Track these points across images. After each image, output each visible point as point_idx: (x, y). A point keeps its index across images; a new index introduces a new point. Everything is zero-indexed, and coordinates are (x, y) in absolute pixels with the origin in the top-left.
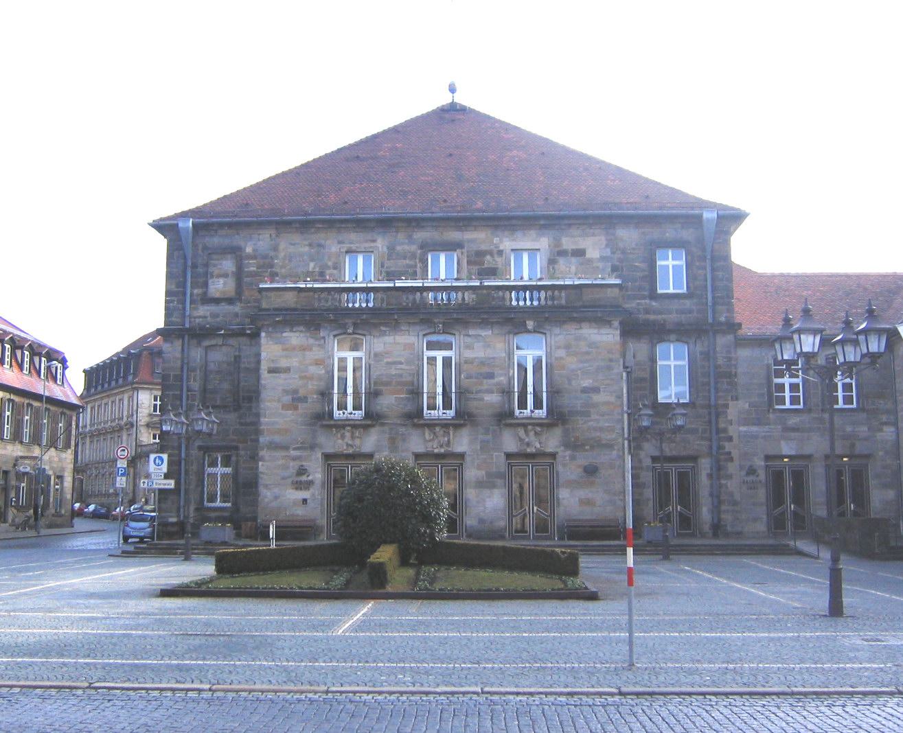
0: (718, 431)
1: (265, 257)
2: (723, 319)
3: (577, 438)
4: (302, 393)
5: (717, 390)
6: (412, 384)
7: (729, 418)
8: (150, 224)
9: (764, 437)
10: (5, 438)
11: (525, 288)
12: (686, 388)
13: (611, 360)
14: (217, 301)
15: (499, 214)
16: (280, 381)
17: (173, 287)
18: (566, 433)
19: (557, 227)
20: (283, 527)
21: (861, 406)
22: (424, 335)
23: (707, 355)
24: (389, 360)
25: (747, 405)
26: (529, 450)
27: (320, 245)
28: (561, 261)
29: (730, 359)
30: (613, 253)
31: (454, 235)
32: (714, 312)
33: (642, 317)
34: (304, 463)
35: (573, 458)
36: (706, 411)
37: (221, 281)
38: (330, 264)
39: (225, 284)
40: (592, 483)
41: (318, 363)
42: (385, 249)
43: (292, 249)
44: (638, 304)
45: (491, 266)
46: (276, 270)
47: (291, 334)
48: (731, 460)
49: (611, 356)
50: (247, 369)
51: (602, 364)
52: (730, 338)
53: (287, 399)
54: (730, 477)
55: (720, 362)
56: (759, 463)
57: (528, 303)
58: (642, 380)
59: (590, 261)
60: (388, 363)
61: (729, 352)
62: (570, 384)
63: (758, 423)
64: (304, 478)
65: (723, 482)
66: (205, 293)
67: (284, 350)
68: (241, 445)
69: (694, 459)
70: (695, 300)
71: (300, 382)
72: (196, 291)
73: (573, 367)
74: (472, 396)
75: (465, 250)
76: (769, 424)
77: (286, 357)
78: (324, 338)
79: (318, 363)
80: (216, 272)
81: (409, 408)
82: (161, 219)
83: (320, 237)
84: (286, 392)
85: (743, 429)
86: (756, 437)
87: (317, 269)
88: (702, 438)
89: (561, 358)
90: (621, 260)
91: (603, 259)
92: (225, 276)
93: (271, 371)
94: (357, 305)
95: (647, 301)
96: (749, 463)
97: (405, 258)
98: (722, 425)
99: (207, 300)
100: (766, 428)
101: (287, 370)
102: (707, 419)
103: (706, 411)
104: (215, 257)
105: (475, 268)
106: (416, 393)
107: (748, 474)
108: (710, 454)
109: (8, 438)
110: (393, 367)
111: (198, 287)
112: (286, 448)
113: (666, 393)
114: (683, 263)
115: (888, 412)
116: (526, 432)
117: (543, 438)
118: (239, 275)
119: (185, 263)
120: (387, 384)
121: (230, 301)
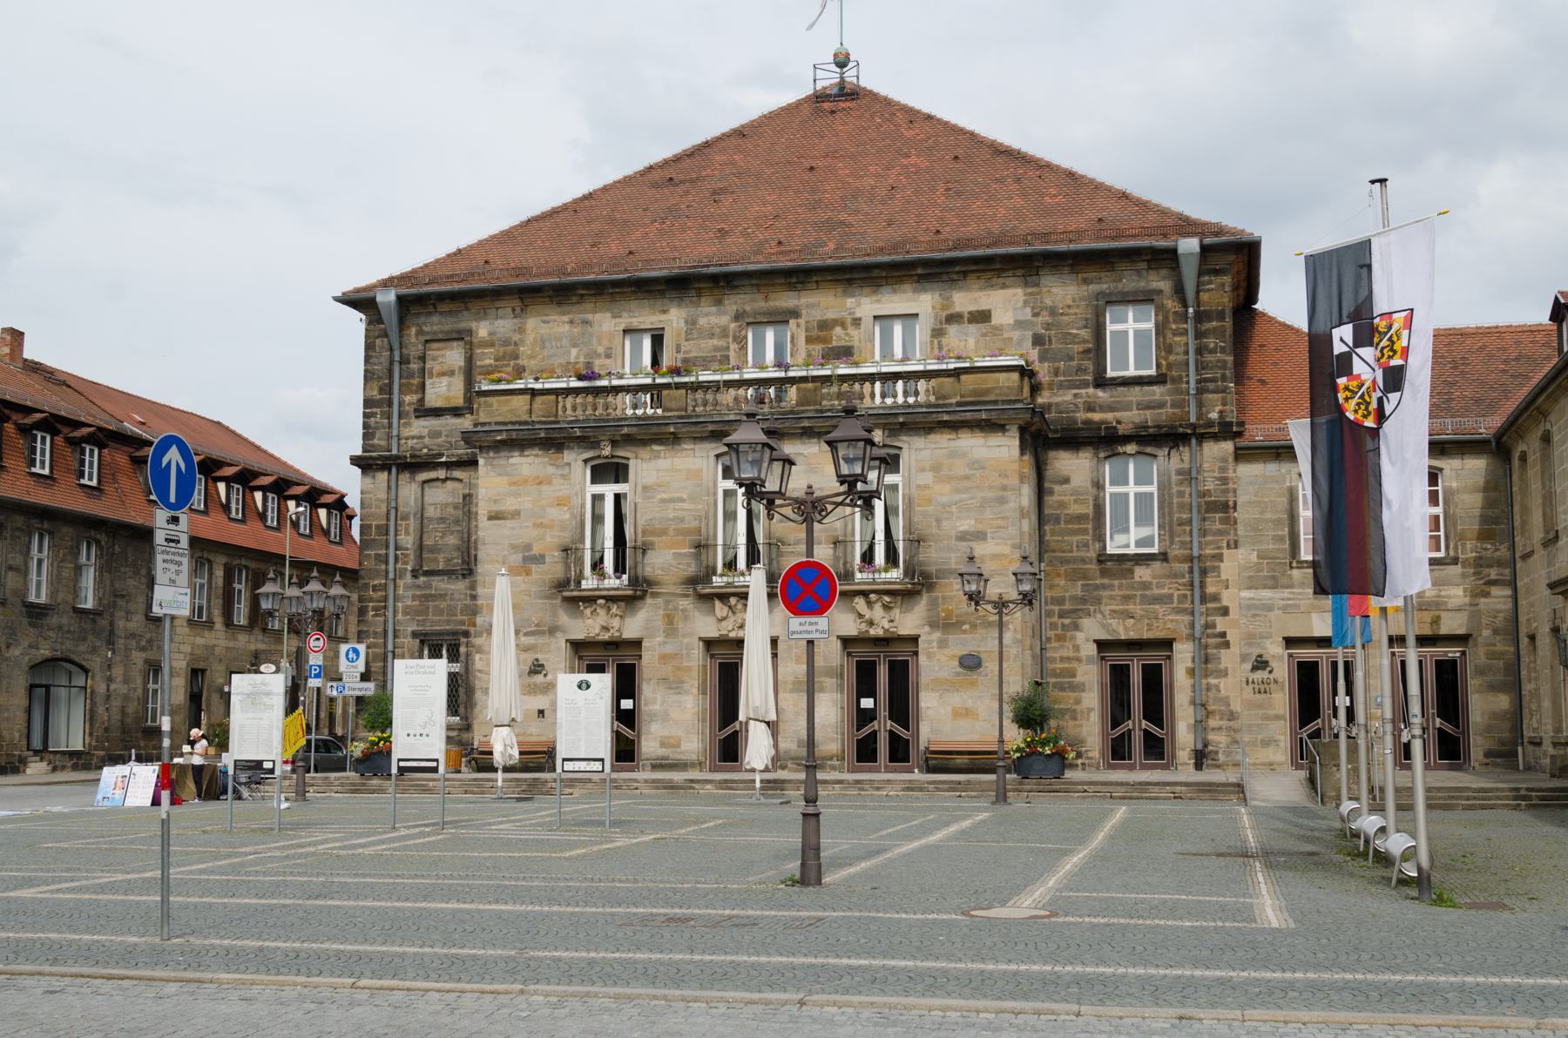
0: (1204, 599)
1: (506, 343)
2: (1214, 415)
3: (949, 613)
4: (536, 550)
5: (1203, 533)
6: (699, 531)
7: (1223, 577)
8: (337, 299)
9: (1285, 609)
11: (896, 376)
12: (1154, 531)
13: (1004, 488)
14: (437, 412)
16: (505, 529)
17: (375, 392)
18: (933, 604)
19: (945, 277)
20: (1439, 789)
21: (1452, 553)
22: (718, 456)
23: (1188, 476)
24: (665, 496)
25: (1254, 557)
26: (872, 632)
27: (585, 322)
28: (953, 330)
29: (1224, 481)
30: (1035, 315)
31: (785, 300)
32: (1200, 405)
33: (1081, 416)
34: (539, 656)
35: (943, 644)
36: (1186, 566)
37: (445, 380)
38: (601, 350)
39: (449, 385)
40: (973, 684)
41: (560, 502)
42: (682, 324)
44: (1075, 395)
45: (843, 343)
47: (523, 460)
48: (1227, 645)
49: (1005, 482)
51: (990, 494)
52: (1228, 446)
53: (516, 558)
54: (1224, 673)
55: (1210, 486)
56: (1274, 649)
57: (878, 400)
58: (1080, 518)
59: (998, 329)
60: (663, 501)
61: (1223, 469)
62: (939, 527)
63: (1274, 583)
64: (539, 678)
65: (1213, 681)
66: (422, 400)
69: (1167, 644)
70: (1169, 386)
71: (535, 533)
72: (408, 399)
73: (944, 500)
74: (790, 549)
75: (802, 321)
76: (1291, 586)
77: (516, 495)
78: (569, 464)
79: (560, 502)
80: (437, 368)
81: (692, 570)
82: (358, 291)
84: (514, 547)
85: (1245, 594)
86: (1270, 608)
87: (582, 359)
88: (1178, 611)
89: (927, 487)
90: (1048, 326)
91: (1019, 324)
93: (495, 517)
94: (900, 400)
95: (1091, 390)
96: (1255, 651)
97: (712, 336)
98: (1210, 589)
99: (424, 412)
100: (1286, 593)
101: (516, 514)
102: (1186, 580)
103: (1186, 566)
104: (435, 345)
105: (818, 349)
106: (702, 546)
107: (1254, 669)
108: (1192, 637)
110: (671, 506)
111: (411, 392)
113: (1120, 539)
114: (1150, 325)
115: (1499, 563)
116: (870, 604)
117: (896, 613)
118: (469, 373)
119: (392, 356)
120: (663, 533)
121: (456, 412)
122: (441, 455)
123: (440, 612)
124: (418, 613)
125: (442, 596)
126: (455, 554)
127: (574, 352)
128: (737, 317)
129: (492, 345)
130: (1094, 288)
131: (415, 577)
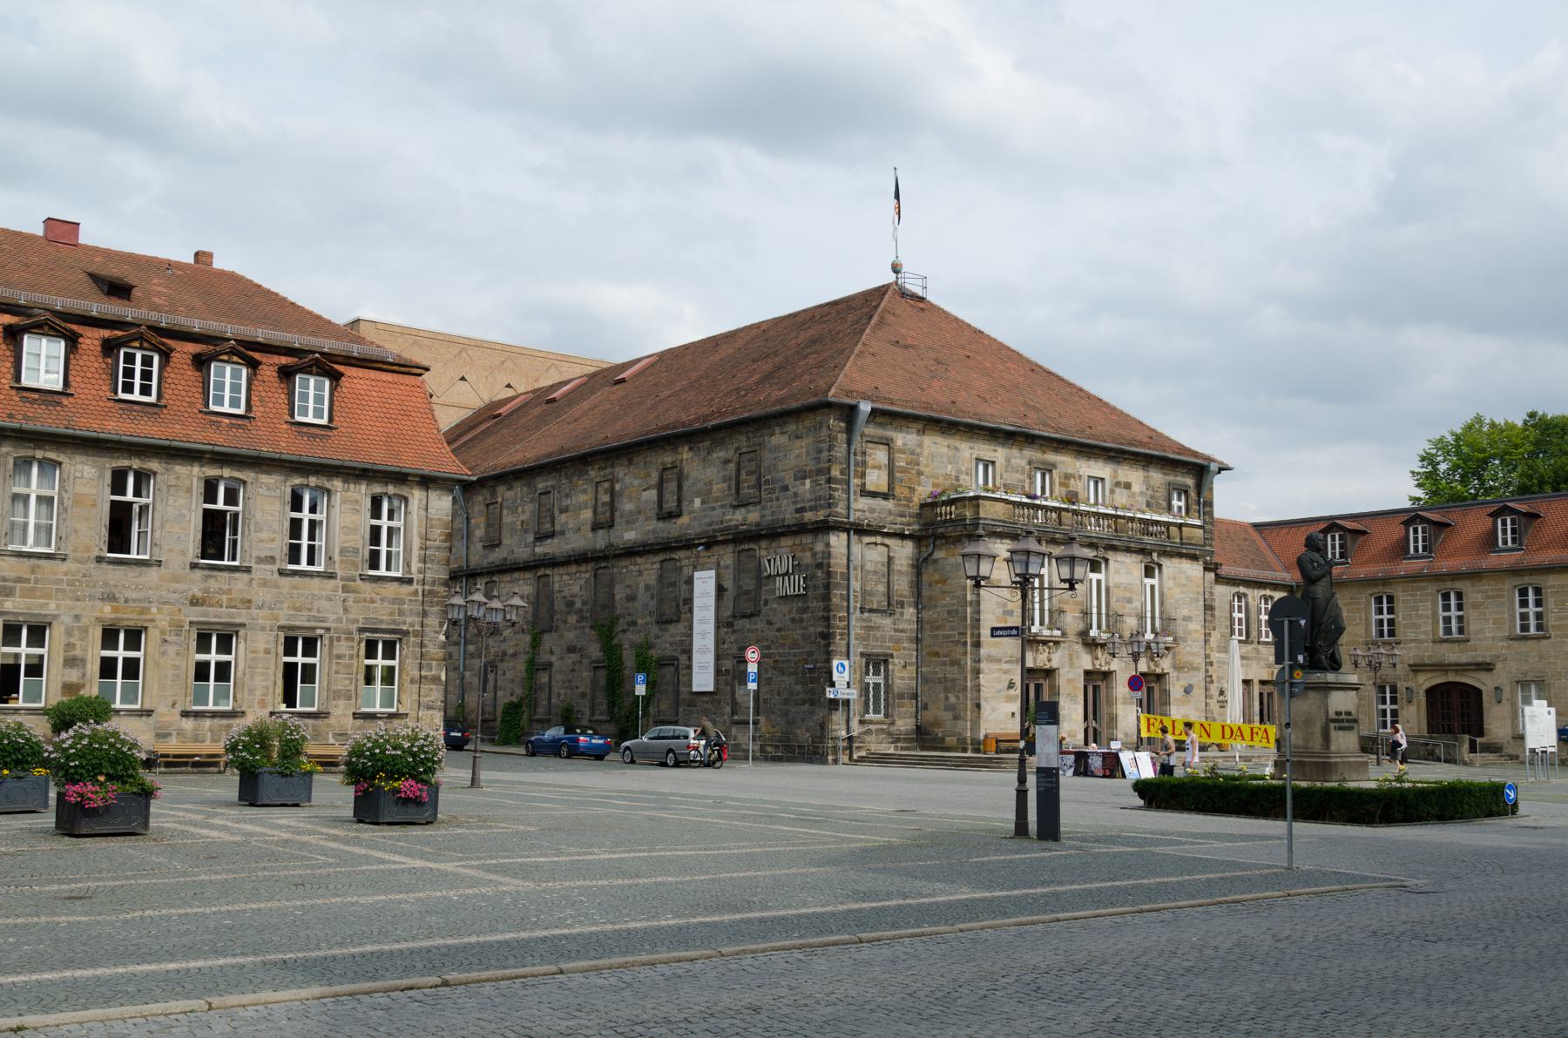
14: (874, 495)
28: (1118, 490)
37: (876, 472)
66: (864, 485)
91: (1142, 493)
92: (879, 468)
99: (865, 493)
112: (999, 661)
121: (885, 496)
124: (864, 639)
125: (877, 628)
128: (1030, 463)
130: (1171, 478)
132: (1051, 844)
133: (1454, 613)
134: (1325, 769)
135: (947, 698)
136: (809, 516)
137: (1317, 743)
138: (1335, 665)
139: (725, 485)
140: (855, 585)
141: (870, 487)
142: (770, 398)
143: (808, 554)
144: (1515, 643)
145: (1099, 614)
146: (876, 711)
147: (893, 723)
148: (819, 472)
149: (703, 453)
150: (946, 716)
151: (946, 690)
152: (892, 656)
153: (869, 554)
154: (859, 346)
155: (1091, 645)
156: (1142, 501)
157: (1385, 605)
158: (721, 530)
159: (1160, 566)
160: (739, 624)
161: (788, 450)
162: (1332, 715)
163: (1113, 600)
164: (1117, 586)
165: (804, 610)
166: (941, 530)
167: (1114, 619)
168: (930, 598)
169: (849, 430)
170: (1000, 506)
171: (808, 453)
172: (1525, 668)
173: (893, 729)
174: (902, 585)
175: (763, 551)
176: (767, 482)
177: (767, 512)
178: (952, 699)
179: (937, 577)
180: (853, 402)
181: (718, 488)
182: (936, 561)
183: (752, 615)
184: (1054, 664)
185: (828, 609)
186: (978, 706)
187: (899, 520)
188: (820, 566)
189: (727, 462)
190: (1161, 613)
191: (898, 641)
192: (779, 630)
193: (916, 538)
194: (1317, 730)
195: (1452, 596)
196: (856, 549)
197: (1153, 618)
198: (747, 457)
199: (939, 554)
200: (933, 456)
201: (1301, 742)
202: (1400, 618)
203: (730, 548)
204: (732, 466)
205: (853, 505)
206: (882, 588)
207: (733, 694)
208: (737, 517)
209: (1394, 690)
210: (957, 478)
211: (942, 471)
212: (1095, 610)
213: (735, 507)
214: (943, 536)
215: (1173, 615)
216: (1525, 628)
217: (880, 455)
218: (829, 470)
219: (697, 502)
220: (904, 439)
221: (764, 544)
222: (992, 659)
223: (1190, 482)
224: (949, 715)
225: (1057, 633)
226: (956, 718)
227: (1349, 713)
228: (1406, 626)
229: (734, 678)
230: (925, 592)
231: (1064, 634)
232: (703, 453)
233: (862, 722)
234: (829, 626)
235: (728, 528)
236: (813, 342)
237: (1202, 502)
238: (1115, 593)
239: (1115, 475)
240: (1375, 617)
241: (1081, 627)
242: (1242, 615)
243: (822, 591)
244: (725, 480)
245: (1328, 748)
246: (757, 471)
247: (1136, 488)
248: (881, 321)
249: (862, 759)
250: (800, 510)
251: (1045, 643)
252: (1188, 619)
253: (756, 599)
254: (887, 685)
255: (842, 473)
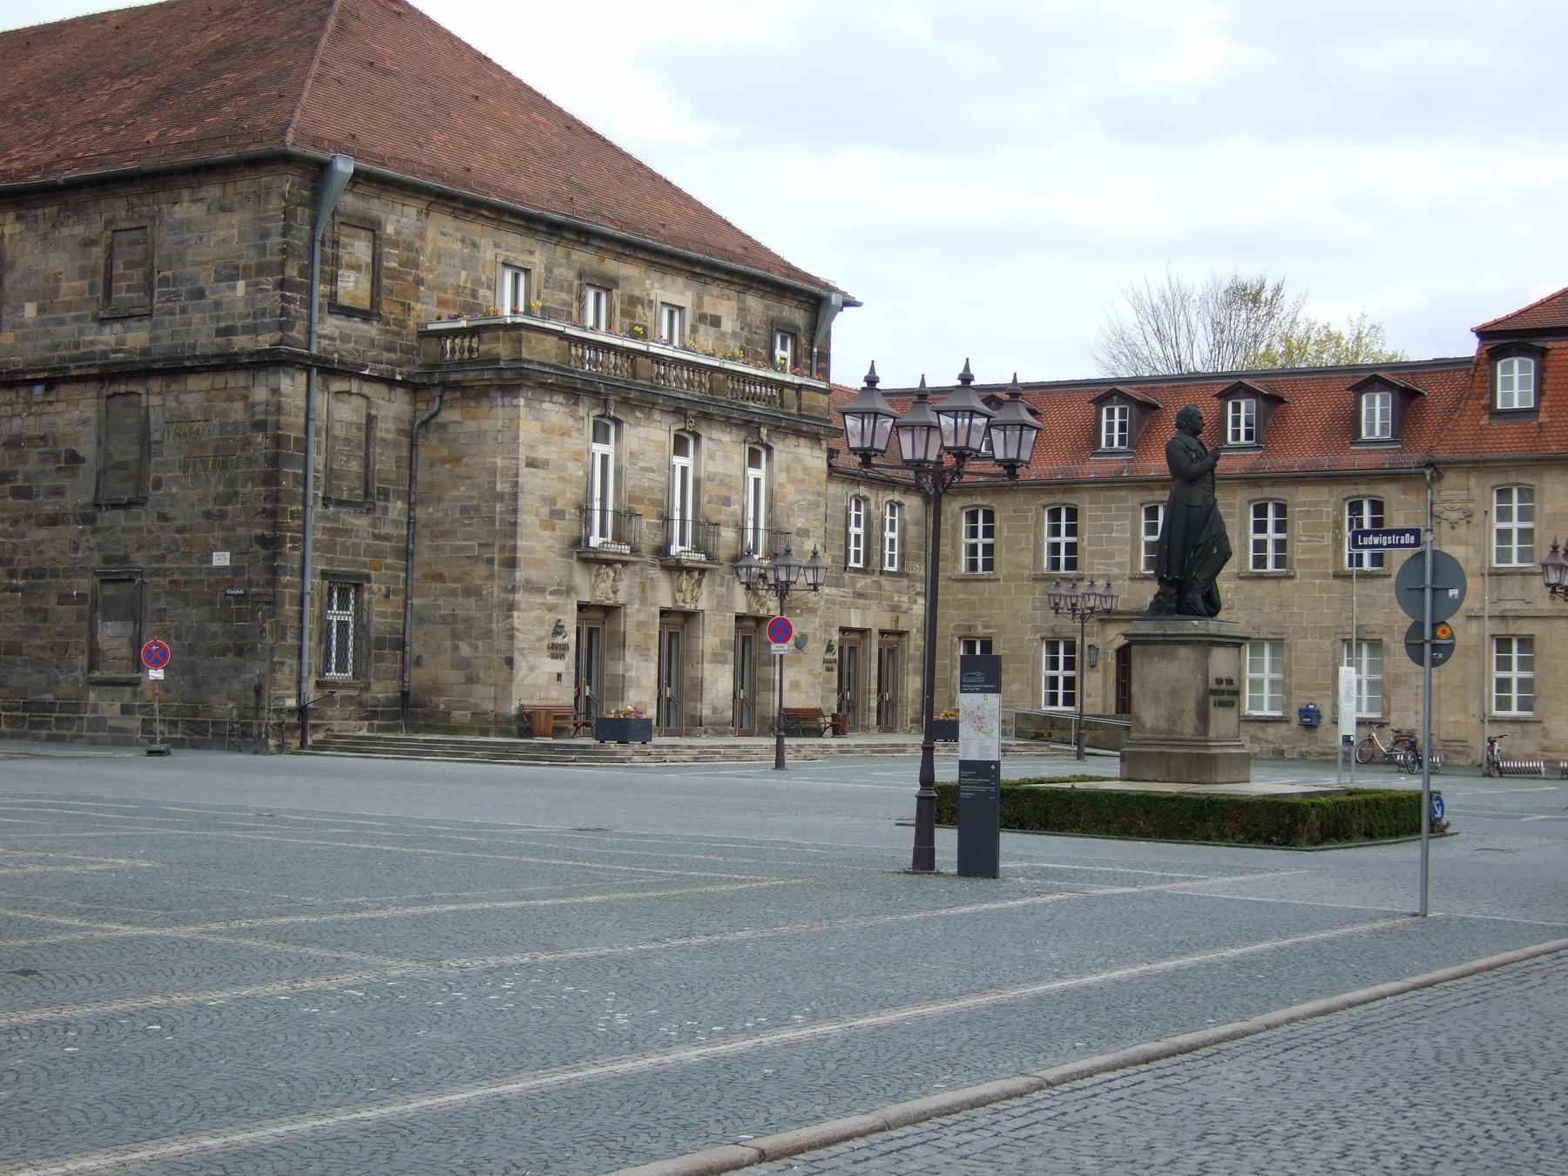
10: (887, 568)
14: (349, 312)
15: (183, 158)
27: (474, 245)
28: (702, 328)
37: (352, 275)
38: (484, 278)
41: (577, 458)
43: (441, 242)
46: (423, 274)
50: (383, 440)
59: (723, 334)
66: (334, 295)
67: (544, 431)
68: (373, 574)
77: (546, 443)
83: (474, 229)
84: (543, 498)
91: (734, 334)
93: (532, 464)
99: (336, 308)
109: (895, 569)
112: (541, 590)
121: (366, 316)
122: (366, 366)
123: (345, 550)
125: (347, 532)
126: (357, 484)
127: (464, 274)
128: (580, 276)
129: (397, 246)
131: (325, 506)
132: (982, 883)
133: (1271, 535)
134: (1203, 764)
135: (456, 648)
136: (241, 342)
137: (1188, 726)
138: (1212, 606)
139: (85, 283)
140: (317, 460)
141: (344, 300)
142: (161, 138)
143: (239, 405)
144: (1246, 584)
145: (683, 520)
146: (341, 667)
147: (367, 688)
148: (263, 269)
149: (43, 226)
150: (454, 677)
151: (455, 636)
152: (368, 578)
153: (340, 410)
154: (316, 65)
155: (676, 568)
156: (734, 346)
157: (1063, 523)
158: (74, 359)
159: (769, 449)
160: (105, 517)
161: (210, 233)
162: (1212, 685)
163: (704, 499)
164: (710, 478)
165: (230, 497)
166: (454, 377)
167: (704, 530)
168: (432, 486)
169: (315, 202)
170: (551, 343)
171: (242, 237)
172: (1257, 620)
173: (367, 696)
174: (386, 462)
175: (155, 398)
176: (164, 281)
177: (163, 332)
178: (465, 650)
179: (444, 452)
180: (325, 156)
181: (70, 287)
182: (443, 427)
183: (130, 504)
184: (621, 598)
185: (274, 498)
186: (510, 662)
187: (386, 355)
188: (260, 426)
189: (88, 243)
190: (769, 522)
191: (377, 554)
192: (180, 530)
193: (413, 387)
194: (1190, 706)
195: (1366, 508)
196: (320, 401)
197: (756, 529)
198: (124, 237)
199: (448, 415)
200: (438, 255)
201: (1163, 725)
202: (1084, 542)
203: (91, 390)
204: (98, 251)
205: (317, 328)
206: (355, 467)
207: (92, 635)
208: (107, 338)
209: (1070, 648)
210: (474, 294)
211: (451, 281)
212: (677, 515)
213: (102, 321)
214: (457, 386)
215: (786, 527)
216: (1260, 562)
217: (359, 249)
218: (282, 266)
219: (30, 310)
220: (400, 219)
221: (156, 385)
222: (534, 588)
223: (799, 317)
224: (456, 677)
225: (626, 549)
226: (471, 680)
227: (1230, 682)
228: (1093, 554)
229: (94, 609)
230: (422, 475)
231: (634, 551)
232: (43, 226)
233: (319, 685)
234: (275, 526)
235: (91, 356)
236: (221, 53)
237: (815, 355)
238: (707, 486)
239: (699, 303)
240: (1048, 539)
241: (659, 540)
242: (861, 531)
243: (263, 467)
244: (83, 273)
245: (1206, 732)
246: (147, 263)
247: (727, 326)
248: (342, 27)
249: (321, 746)
250: (228, 331)
251: (608, 563)
252: (804, 533)
253: (140, 477)
254: (361, 627)
255: (302, 273)
